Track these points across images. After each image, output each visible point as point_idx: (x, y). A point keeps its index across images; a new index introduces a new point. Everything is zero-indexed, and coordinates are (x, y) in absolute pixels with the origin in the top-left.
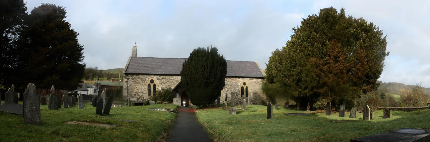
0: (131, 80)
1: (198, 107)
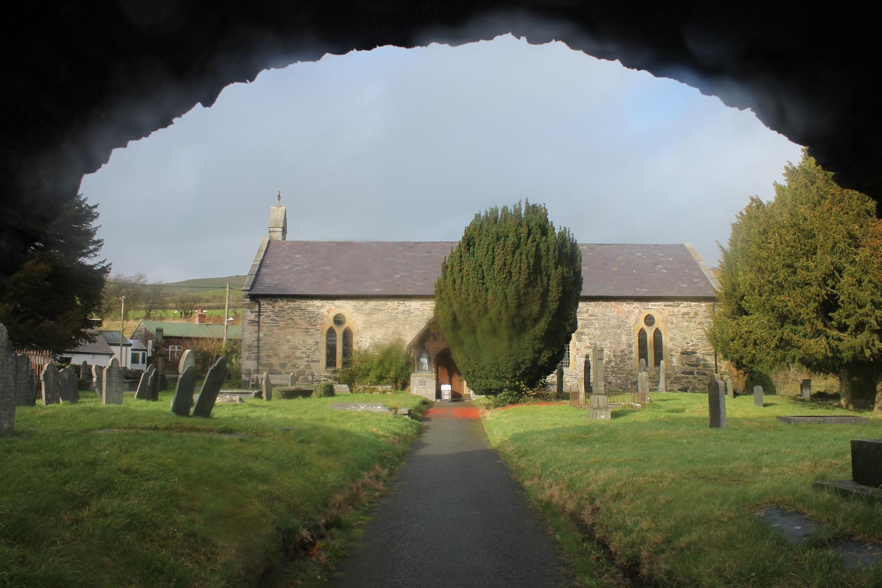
0: (269, 316)
1: (491, 402)
